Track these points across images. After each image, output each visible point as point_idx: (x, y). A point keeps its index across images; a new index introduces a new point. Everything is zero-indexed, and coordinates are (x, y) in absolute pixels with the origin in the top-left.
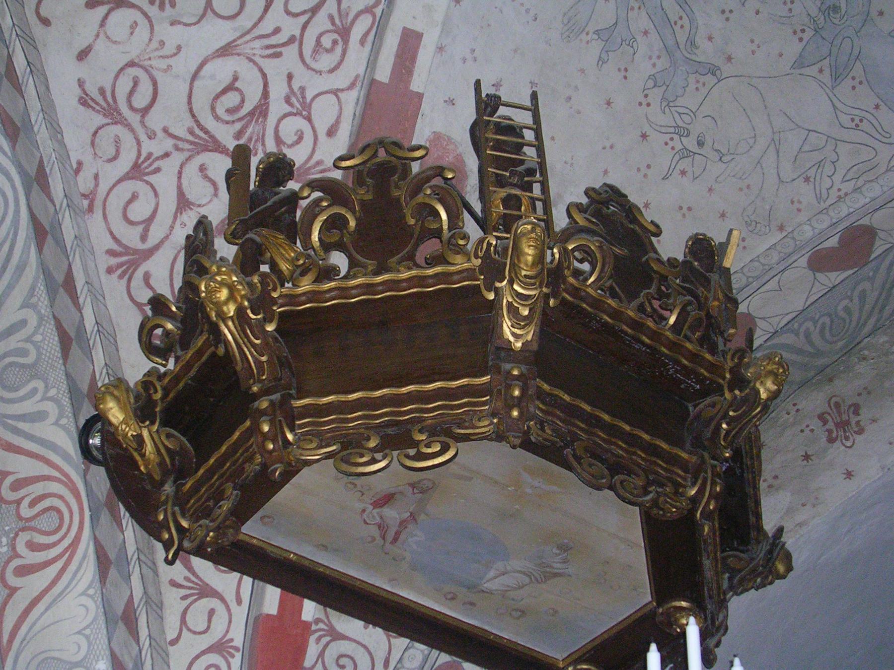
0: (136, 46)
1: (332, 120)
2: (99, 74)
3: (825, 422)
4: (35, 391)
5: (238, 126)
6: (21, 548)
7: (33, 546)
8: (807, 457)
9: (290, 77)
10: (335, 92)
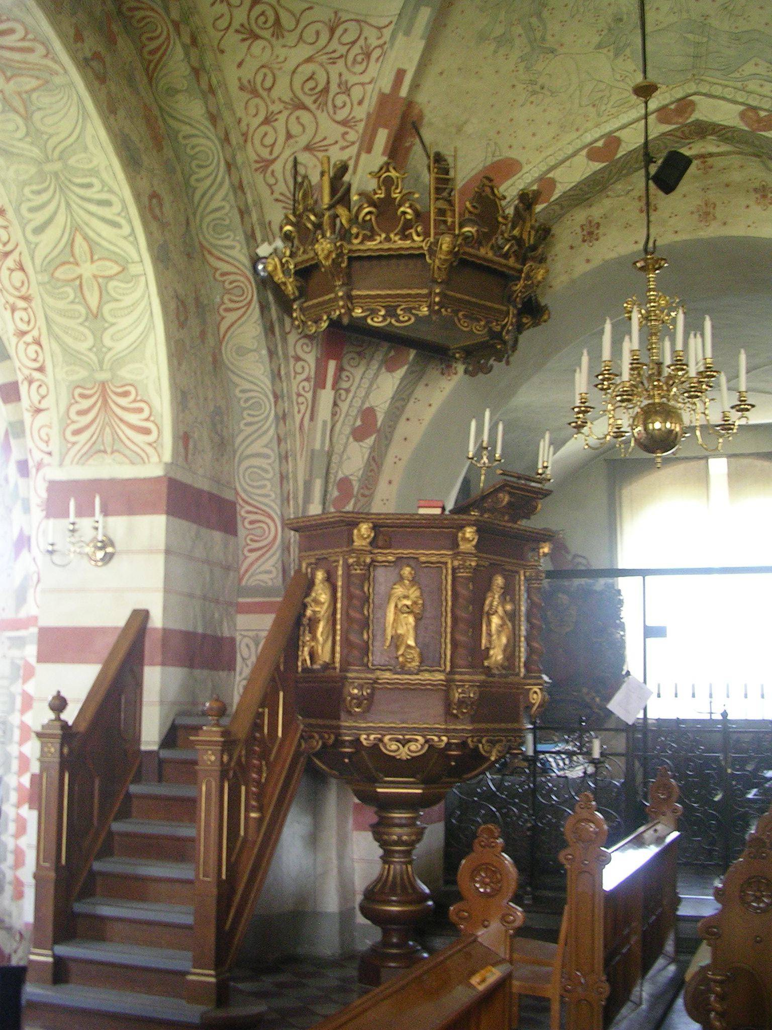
0: (266, 57)
1: (361, 97)
2: (247, 73)
3: (583, 230)
4: (228, 237)
5: (315, 97)
6: (226, 301)
7: (231, 301)
8: (572, 248)
9: (340, 75)
10: (363, 84)
